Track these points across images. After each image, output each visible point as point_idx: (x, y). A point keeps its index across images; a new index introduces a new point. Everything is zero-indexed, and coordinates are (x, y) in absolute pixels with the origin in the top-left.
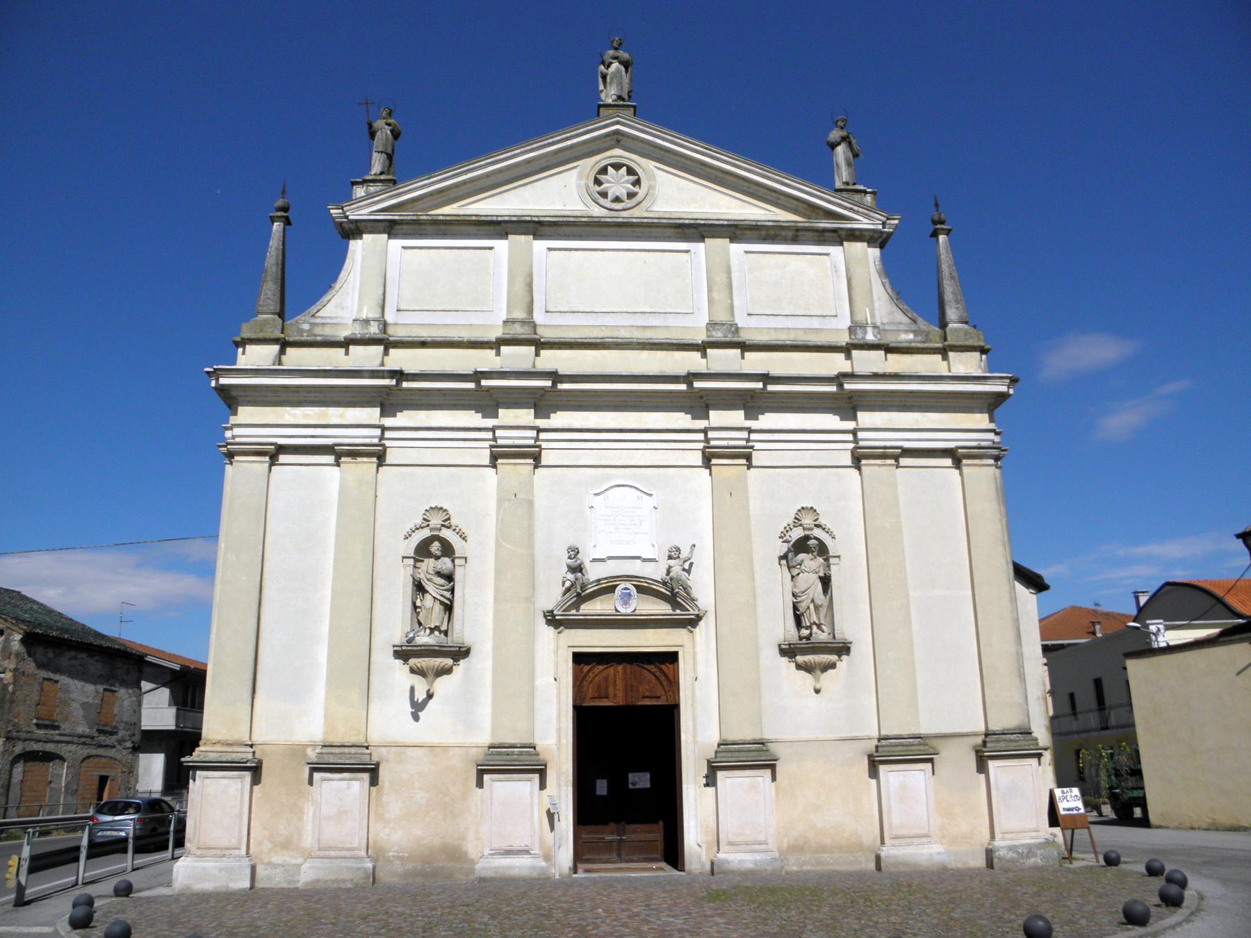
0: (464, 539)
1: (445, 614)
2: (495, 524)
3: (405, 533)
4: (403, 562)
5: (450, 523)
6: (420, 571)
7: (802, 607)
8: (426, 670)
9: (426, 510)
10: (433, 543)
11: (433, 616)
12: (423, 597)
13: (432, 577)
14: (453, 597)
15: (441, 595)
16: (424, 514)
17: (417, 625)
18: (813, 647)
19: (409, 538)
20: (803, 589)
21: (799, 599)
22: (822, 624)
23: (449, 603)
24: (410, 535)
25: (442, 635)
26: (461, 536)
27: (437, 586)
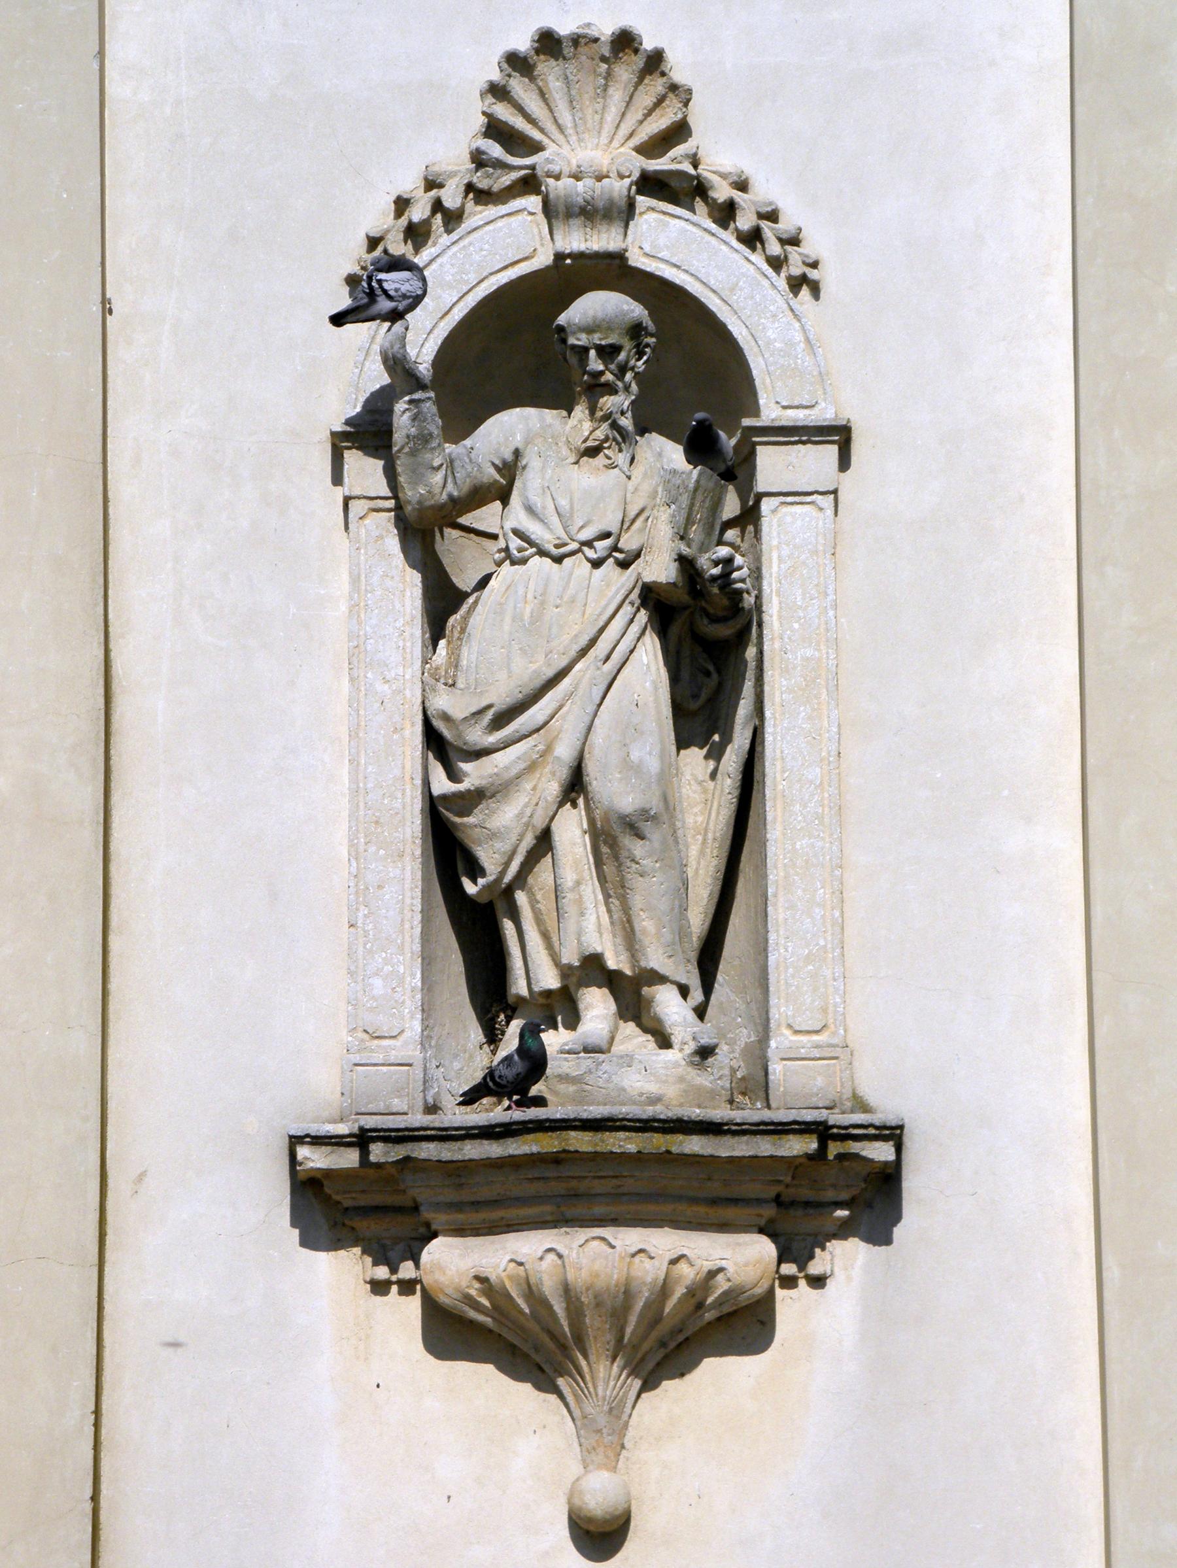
4: (337, 479)
7: (494, 835)
18: (557, 1159)
20: (500, 695)
21: (474, 774)
22: (657, 978)
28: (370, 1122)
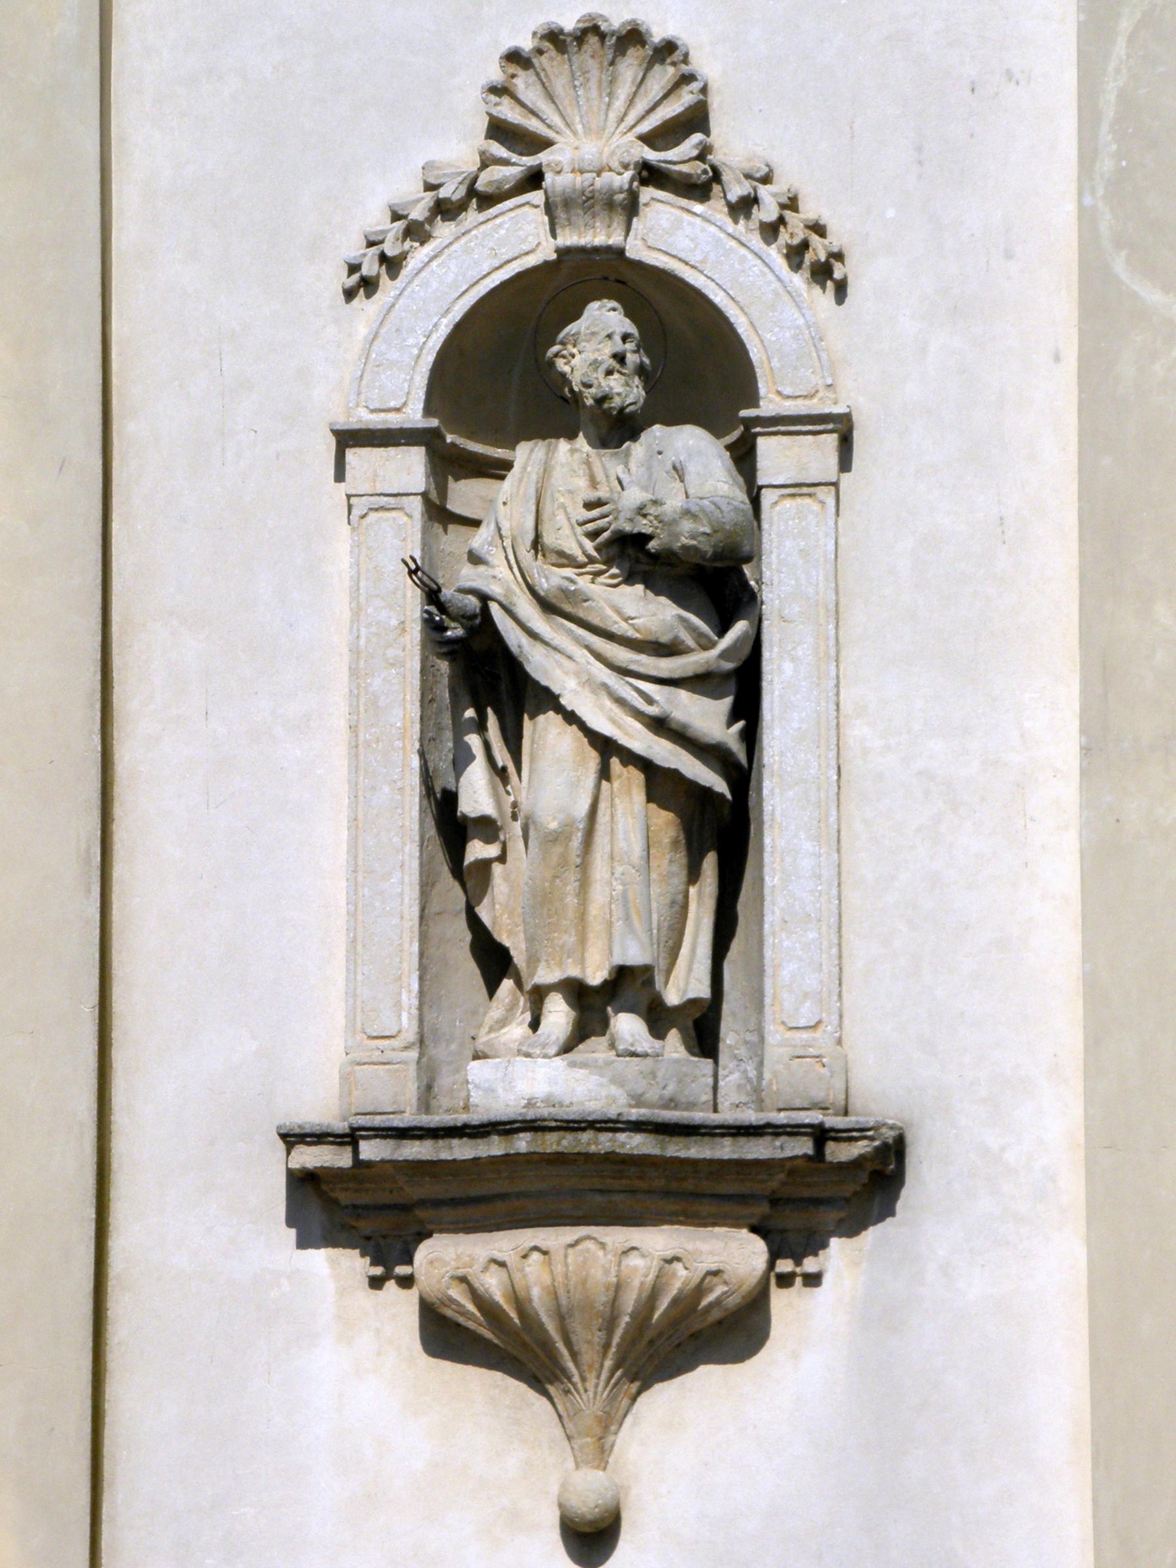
0: (822, 273)
1: (693, 874)
2: (1069, 147)
3: (353, 248)
4: (340, 476)
5: (703, 154)
6: (480, 539)
8: (551, 1327)
9: (514, 57)
10: (576, 314)
11: (599, 895)
12: (514, 742)
13: (584, 583)
14: (751, 737)
15: (660, 725)
16: (498, 90)
17: (469, 970)
19: (388, 289)
23: (719, 785)
24: (392, 265)
25: (674, 1045)
26: (796, 254)
27: (623, 655)
28: (362, 1121)
